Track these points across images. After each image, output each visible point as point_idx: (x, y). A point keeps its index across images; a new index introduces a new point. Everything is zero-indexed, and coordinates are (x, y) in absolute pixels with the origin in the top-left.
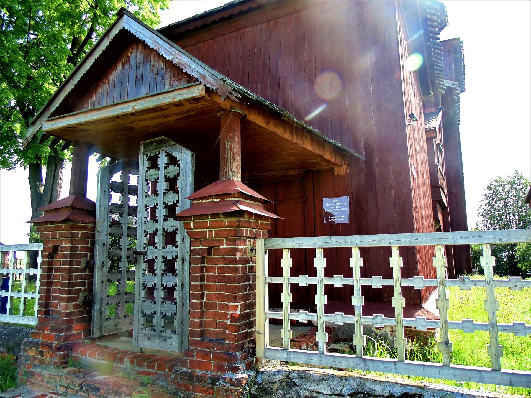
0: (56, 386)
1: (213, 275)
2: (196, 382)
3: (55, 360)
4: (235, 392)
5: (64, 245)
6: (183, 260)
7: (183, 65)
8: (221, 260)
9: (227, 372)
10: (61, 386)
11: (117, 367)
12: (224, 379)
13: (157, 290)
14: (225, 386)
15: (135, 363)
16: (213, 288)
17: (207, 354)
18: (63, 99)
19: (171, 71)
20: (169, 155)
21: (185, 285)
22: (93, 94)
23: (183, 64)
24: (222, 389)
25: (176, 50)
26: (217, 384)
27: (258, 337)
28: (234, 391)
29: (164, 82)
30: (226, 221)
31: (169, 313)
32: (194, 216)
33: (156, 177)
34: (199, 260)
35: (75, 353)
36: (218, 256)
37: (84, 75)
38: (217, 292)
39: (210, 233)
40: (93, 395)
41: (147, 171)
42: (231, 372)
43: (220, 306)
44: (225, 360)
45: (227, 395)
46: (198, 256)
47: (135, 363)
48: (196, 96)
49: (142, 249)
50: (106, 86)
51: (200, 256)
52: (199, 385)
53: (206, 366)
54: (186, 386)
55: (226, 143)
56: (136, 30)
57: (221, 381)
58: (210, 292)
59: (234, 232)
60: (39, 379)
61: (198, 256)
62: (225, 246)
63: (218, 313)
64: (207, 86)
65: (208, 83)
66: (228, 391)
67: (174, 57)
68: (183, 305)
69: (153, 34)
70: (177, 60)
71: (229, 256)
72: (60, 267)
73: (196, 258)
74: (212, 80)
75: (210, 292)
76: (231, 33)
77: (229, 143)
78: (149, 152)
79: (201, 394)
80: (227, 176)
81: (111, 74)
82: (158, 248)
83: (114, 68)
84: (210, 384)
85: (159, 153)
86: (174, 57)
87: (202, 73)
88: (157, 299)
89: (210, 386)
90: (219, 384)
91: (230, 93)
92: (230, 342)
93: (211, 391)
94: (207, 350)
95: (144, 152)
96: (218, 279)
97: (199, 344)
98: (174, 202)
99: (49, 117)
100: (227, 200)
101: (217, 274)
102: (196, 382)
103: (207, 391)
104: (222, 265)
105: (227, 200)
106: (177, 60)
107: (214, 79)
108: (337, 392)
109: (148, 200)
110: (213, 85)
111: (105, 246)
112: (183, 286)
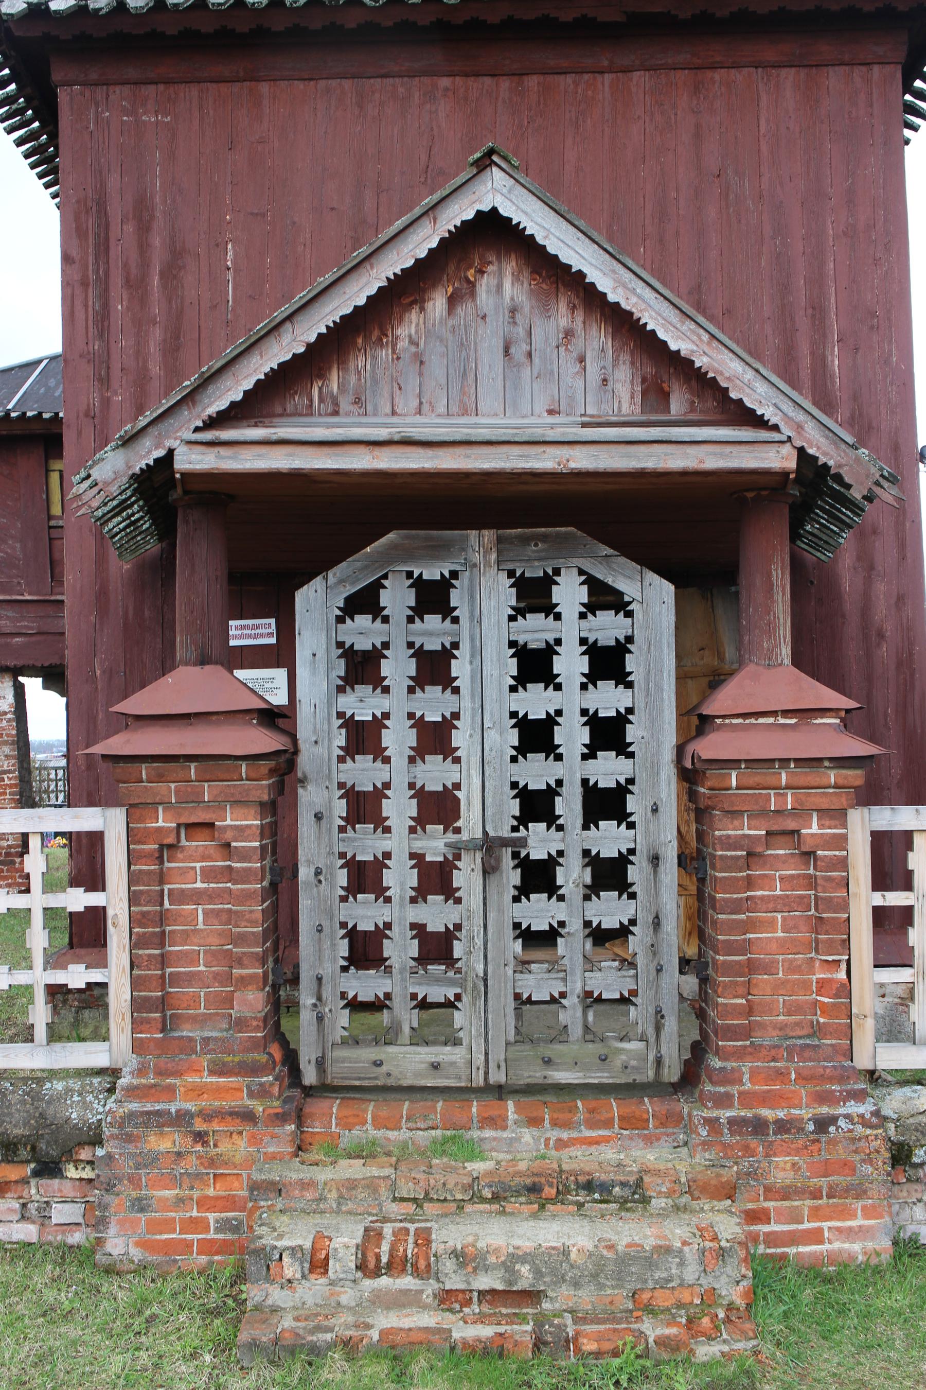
0: (380, 1205)
1: (768, 896)
2: (775, 1134)
3: (271, 1149)
4: (876, 1139)
5: (228, 822)
6: (655, 860)
7: (729, 379)
8: (792, 860)
9: (844, 1104)
10: (395, 1199)
11: (482, 1140)
12: (847, 1117)
13: (569, 939)
14: (850, 1131)
15: (547, 1122)
16: (771, 925)
17: (781, 1075)
18: (259, 381)
19: (632, 363)
20: (594, 585)
21: (664, 922)
22: (330, 368)
23: (727, 375)
24: (844, 1137)
25: (702, 331)
26: (832, 1129)
27: (859, 1026)
28: (873, 1138)
29: (610, 387)
30: (832, 776)
31: (614, 991)
32: (746, 761)
33: (551, 637)
34: (742, 862)
35: (317, 1124)
36: (781, 852)
37: (342, 318)
38: (780, 934)
39: (780, 798)
40: (521, 1204)
41: (512, 618)
42: (853, 1102)
43: (786, 964)
44: (831, 1080)
45: (857, 1148)
46: (739, 853)
47: (547, 1122)
48: (771, 468)
49: (506, 833)
50: (385, 354)
51: (745, 853)
52: (782, 1140)
53: (787, 1098)
54: (746, 1148)
55: (774, 573)
56: (548, 230)
57: (842, 1123)
58: (760, 935)
59: (847, 800)
60: (309, 1195)
61: (739, 853)
62: (815, 829)
63: (784, 983)
64: (811, 451)
65: (811, 447)
66: (860, 1139)
67: (695, 348)
68: (659, 970)
69: (615, 262)
70: (705, 359)
71: (826, 853)
72: (195, 886)
73: (732, 857)
74: (822, 440)
75: (760, 935)
76: (382, 76)
77: (779, 572)
78: (518, 564)
79: (787, 1158)
80: (777, 654)
81: (400, 320)
82: (568, 827)
83: (414, 302)
84: (812, 1133)
85: (557, 572)
86: (695, 348)
87: (791, 414)
88: (571, 958)
89: (812, 1137)
90: (837, 1130)
91: (877, 484)
92: (834, 1042)
93: (815, 1148)
94: (772, 1064)
95: (498, 562)
96: (785, 905)
97: (751, 1054)
98: (618, 711)
99: (197, 430)
100: (815, 722)
101: (778, 892)
102: (775, 1134)
103: (806, 1147)
104: (793, 872)
105: (815, 722)
106: (705, 359)
107: (827, 438)
108: (442, 1198)
109: (523, 700)
110: (825, 454)
111: (324, 822)
112: (657, 923)
